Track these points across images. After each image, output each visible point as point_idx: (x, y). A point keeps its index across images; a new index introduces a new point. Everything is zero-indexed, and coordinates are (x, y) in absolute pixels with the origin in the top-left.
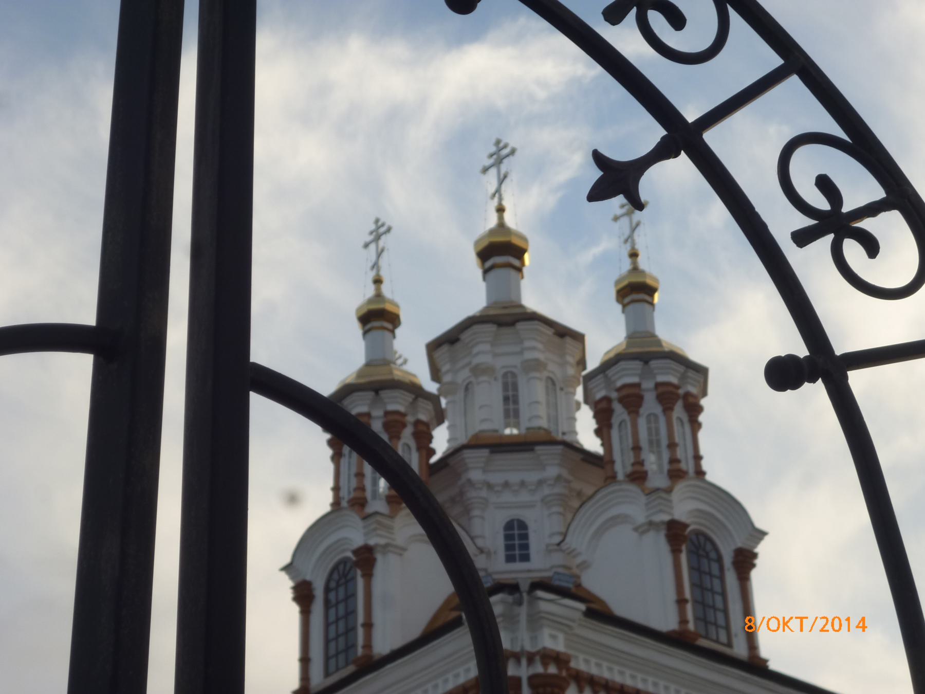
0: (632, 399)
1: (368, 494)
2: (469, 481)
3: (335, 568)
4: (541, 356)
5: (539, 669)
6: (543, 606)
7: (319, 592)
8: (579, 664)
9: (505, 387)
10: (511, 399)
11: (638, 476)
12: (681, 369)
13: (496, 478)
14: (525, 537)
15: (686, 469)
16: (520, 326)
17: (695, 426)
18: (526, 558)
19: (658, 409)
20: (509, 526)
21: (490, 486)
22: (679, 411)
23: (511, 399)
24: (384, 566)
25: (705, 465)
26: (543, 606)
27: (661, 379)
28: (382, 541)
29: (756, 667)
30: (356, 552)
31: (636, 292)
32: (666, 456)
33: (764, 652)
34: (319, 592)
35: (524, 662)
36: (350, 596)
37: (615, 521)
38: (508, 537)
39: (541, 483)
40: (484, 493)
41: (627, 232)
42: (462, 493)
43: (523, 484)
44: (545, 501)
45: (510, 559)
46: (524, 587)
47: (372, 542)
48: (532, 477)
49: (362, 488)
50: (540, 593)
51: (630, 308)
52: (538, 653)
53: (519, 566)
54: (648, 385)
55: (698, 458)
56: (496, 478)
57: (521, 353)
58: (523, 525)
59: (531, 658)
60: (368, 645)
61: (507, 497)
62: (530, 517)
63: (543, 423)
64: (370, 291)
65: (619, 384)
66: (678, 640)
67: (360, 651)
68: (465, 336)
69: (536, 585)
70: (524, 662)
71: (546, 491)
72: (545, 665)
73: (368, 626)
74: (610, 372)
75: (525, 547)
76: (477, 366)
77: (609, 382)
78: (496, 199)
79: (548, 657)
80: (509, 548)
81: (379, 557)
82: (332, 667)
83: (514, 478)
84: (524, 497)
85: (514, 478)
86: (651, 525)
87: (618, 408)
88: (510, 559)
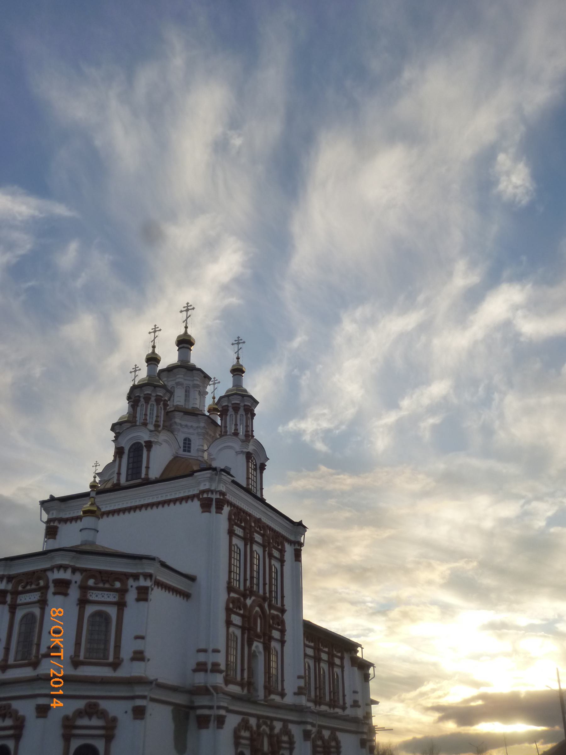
0: (147, 399)
1: (148, 422)
2: (175, 422)
3: (134, 444)
4: (198, 383)
5: (218, 497)
6: (223, 477)
7: (126, 451)
8: (229, 497)
9: (186, 391)
10: (187, 395)
11: (236, 434)
12: (252, 401)
13: (184, 423)
14: (190, 444)
15: (249, 435)
16: (194, 372)
17: (252, 419)
18: (189, 451)
19: (244, 413)
20: (185, 440)
21: (181, 425)
22: (249, 416)
23: (187, 395)
24: (155, 450)
25: (254, 434)
26: (223, 477)
27: (246, 403)
28: (156, 440)
29: (263, 501)
30: (145, 442)
31: (237, 371)
32: (154, 419)
33: (264, 497)
34: (126, 451)
35: (214, 493)
36: (141, 456)
37: (228, 447)
38: (184, 443)
39: (197, 427)
40: (179, 427)
41: (236, 350)
42: (171, 425)
43: (192, 426)
44: (198, 434)
45: (184, 451)
46: (218, 470)
47: (152, 440)
48: (195, 425)
49: (146, 419)
50: (223, 473)
51: (236, 376)
52: (218, 491)
53: (188, 454)
54: (242, 404)
55: (253, 431)
56: (184, 423)
57: (193, 381)
58: (189, 440)
59: (216, 492)
60: (147, 474)
61: (186, 430)
62: (192, 437)
63: (198, 406)
64: (150, 351)
65: (233, 402)
66: (247, 490)
67: (143, 476)
68: (175, 371)
69: (222, 470)
70: (214, 493)
71: (200, 431)
72: (220, 496)
73: (147, 468)
74: (231, 397)
75: (189, 447)
76: (179, 382)
77: (229, 401)
78: (185, 323)
79: (222, 494)
80: (184, 447)
81: (154, 445)
82: (129, 479)
83: (190, 424)
84: (191, 431)
85: (190, 424)
86: (242, 452)
87: (231, 409)
88: (184, 451)
